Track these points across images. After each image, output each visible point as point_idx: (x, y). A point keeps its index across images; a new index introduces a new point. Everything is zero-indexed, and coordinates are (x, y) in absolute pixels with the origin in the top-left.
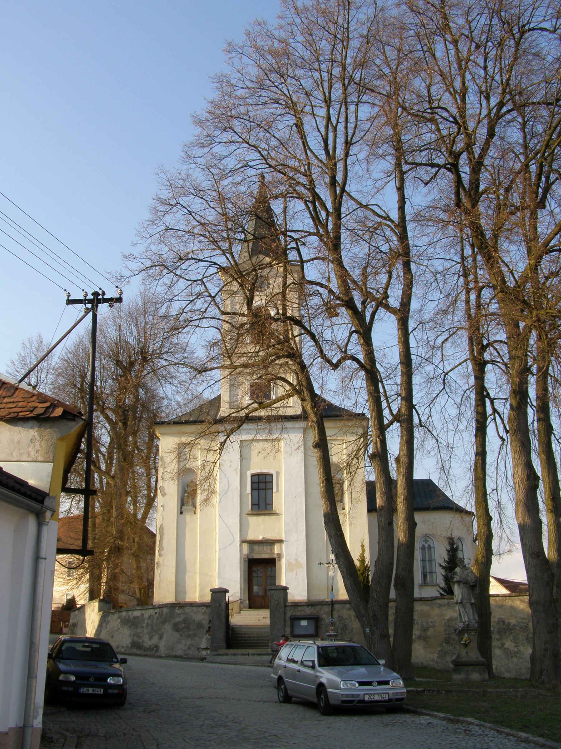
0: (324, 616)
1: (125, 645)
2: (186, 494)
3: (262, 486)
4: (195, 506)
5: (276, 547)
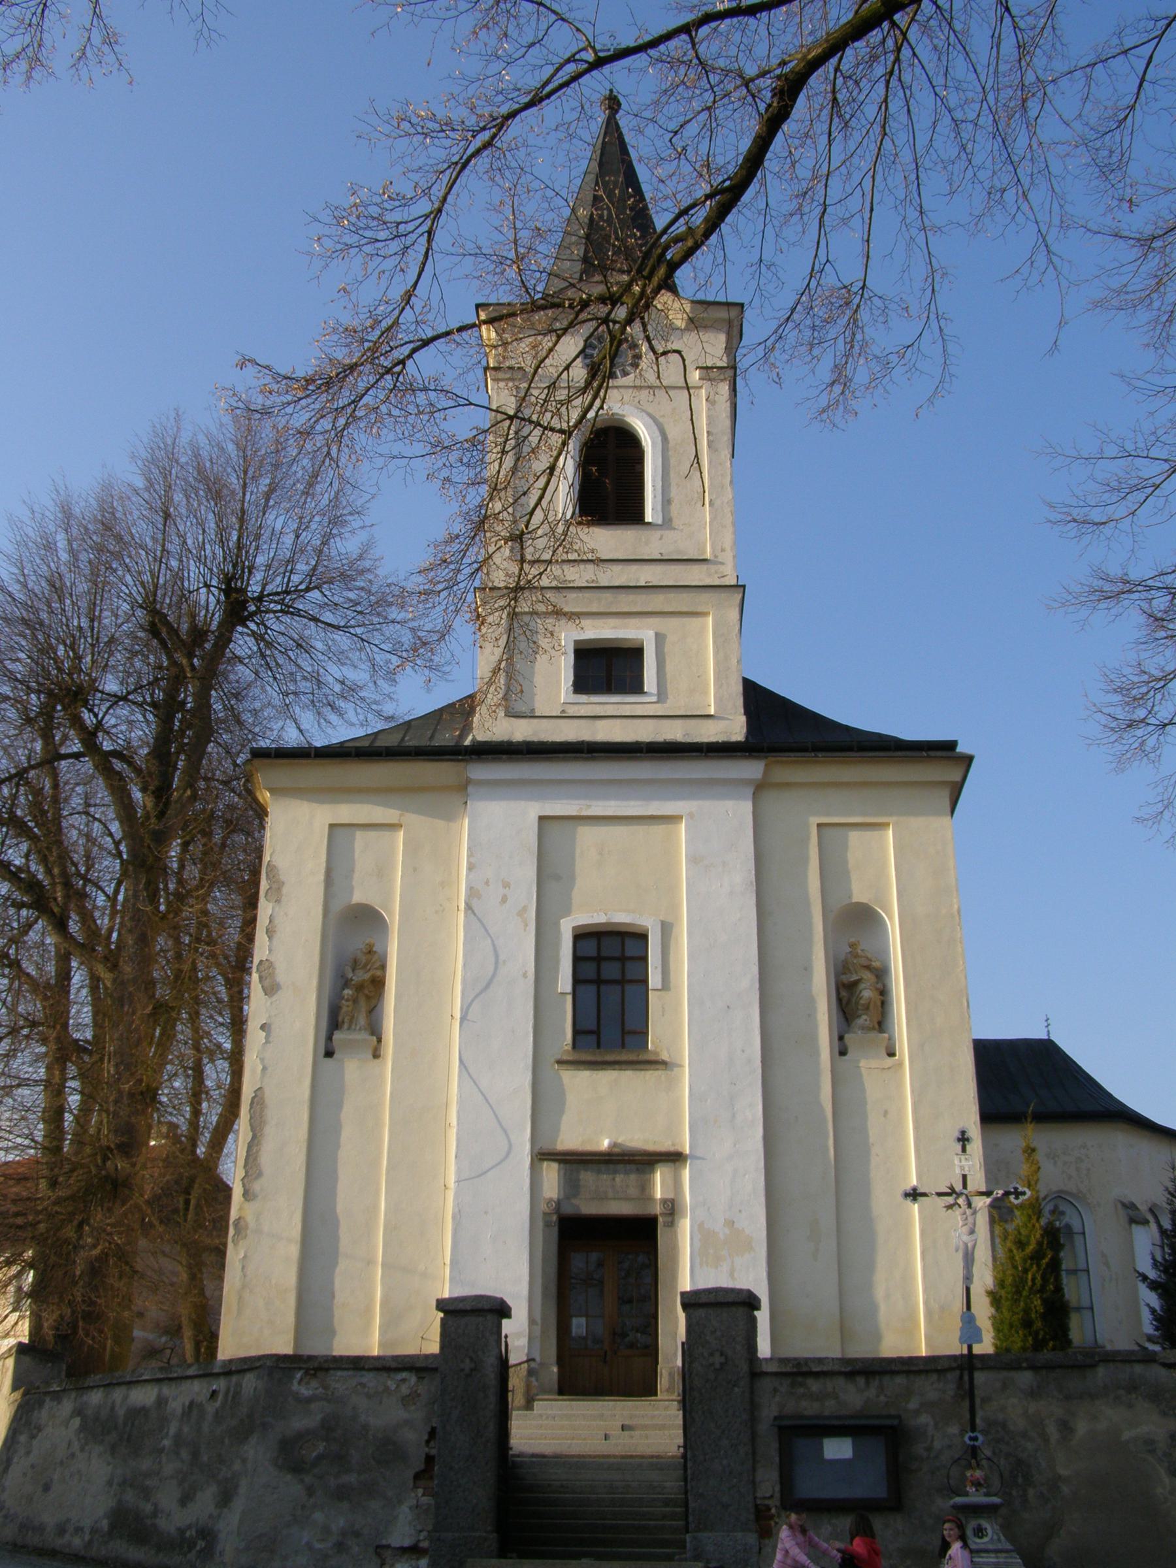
0: (924, 1419)
1: (87, 1523)
2: (347, 992)
3: (611, 970)
4: (376, 1031)
5: (658, 1176)
